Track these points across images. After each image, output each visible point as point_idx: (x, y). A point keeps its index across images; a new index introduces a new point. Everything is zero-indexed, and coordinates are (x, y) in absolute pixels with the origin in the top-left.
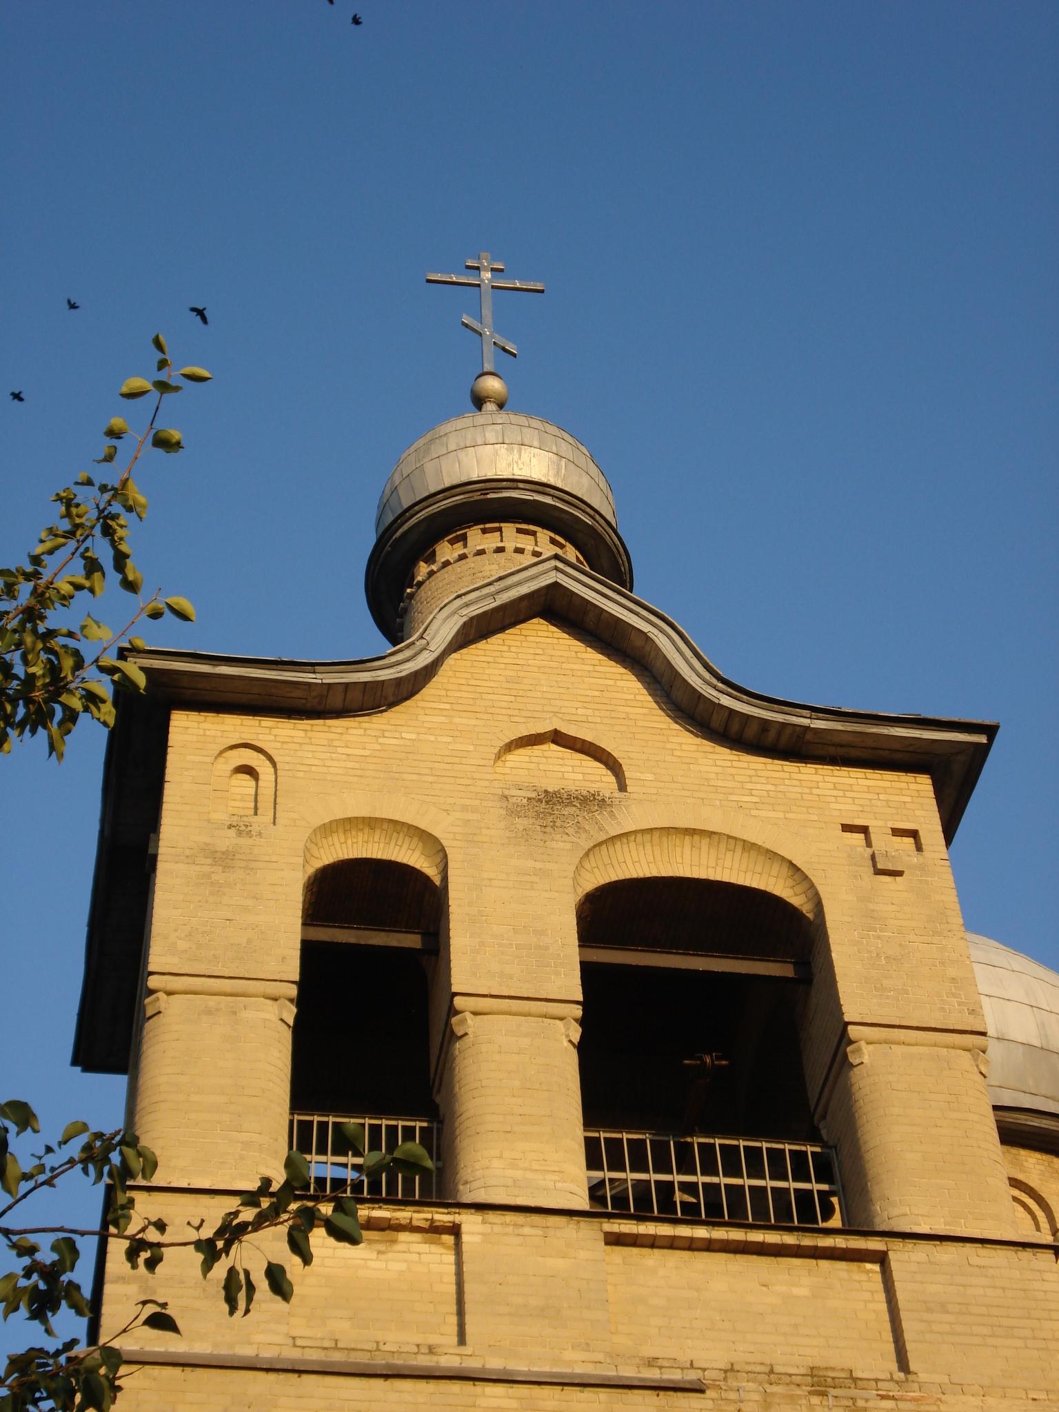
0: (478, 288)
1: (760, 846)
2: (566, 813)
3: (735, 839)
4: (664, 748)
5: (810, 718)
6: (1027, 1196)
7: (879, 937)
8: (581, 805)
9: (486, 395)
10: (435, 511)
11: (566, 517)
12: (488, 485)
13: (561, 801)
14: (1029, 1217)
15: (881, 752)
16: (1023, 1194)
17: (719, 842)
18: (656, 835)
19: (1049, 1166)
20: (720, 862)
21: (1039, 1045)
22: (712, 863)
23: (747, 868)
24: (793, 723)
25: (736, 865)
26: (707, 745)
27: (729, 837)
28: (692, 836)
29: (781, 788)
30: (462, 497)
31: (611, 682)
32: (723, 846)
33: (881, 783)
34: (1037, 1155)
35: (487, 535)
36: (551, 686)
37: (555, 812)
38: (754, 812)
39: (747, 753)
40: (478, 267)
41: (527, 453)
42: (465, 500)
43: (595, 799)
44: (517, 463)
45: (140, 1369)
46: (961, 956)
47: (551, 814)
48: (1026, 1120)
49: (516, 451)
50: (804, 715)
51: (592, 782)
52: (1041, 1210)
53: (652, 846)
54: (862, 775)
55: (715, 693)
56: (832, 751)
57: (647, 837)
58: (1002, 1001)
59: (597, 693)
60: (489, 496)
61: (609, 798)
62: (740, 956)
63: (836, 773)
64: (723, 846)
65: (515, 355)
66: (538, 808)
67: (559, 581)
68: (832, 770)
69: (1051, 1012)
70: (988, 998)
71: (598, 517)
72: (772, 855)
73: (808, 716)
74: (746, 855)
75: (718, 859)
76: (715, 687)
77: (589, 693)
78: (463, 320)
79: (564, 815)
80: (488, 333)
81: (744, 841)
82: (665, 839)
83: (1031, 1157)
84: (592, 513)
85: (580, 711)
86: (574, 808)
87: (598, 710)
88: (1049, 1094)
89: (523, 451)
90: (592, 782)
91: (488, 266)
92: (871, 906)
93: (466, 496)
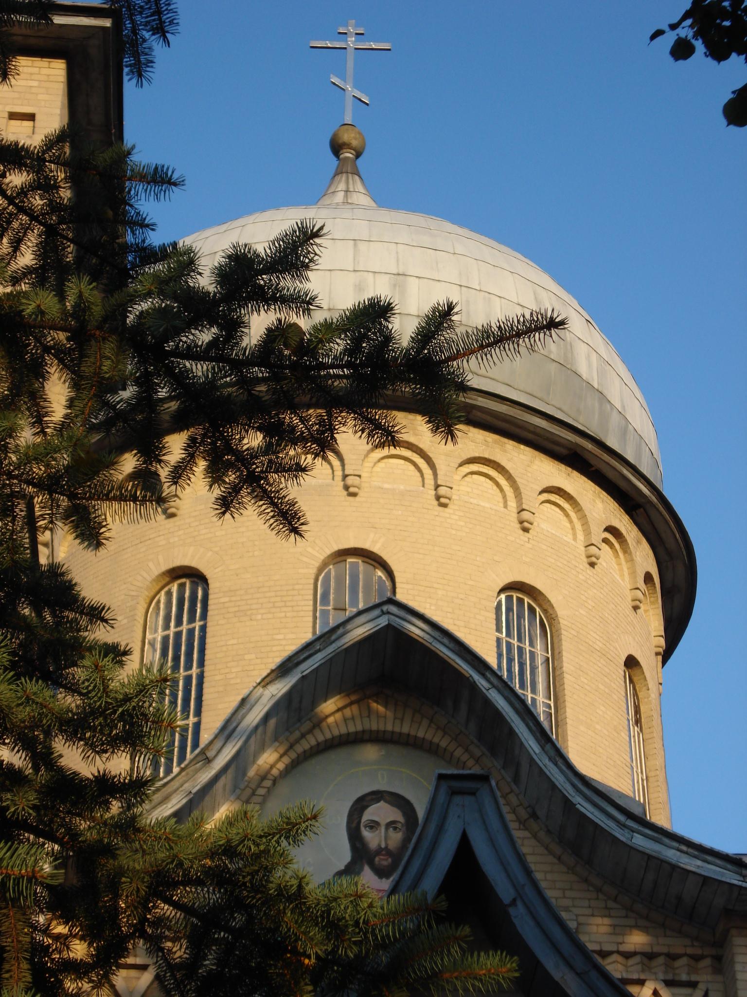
14: (418, 474)
16: (415, 455)
58: (431, 282)
65: (367, 104)
70: (417, 279)
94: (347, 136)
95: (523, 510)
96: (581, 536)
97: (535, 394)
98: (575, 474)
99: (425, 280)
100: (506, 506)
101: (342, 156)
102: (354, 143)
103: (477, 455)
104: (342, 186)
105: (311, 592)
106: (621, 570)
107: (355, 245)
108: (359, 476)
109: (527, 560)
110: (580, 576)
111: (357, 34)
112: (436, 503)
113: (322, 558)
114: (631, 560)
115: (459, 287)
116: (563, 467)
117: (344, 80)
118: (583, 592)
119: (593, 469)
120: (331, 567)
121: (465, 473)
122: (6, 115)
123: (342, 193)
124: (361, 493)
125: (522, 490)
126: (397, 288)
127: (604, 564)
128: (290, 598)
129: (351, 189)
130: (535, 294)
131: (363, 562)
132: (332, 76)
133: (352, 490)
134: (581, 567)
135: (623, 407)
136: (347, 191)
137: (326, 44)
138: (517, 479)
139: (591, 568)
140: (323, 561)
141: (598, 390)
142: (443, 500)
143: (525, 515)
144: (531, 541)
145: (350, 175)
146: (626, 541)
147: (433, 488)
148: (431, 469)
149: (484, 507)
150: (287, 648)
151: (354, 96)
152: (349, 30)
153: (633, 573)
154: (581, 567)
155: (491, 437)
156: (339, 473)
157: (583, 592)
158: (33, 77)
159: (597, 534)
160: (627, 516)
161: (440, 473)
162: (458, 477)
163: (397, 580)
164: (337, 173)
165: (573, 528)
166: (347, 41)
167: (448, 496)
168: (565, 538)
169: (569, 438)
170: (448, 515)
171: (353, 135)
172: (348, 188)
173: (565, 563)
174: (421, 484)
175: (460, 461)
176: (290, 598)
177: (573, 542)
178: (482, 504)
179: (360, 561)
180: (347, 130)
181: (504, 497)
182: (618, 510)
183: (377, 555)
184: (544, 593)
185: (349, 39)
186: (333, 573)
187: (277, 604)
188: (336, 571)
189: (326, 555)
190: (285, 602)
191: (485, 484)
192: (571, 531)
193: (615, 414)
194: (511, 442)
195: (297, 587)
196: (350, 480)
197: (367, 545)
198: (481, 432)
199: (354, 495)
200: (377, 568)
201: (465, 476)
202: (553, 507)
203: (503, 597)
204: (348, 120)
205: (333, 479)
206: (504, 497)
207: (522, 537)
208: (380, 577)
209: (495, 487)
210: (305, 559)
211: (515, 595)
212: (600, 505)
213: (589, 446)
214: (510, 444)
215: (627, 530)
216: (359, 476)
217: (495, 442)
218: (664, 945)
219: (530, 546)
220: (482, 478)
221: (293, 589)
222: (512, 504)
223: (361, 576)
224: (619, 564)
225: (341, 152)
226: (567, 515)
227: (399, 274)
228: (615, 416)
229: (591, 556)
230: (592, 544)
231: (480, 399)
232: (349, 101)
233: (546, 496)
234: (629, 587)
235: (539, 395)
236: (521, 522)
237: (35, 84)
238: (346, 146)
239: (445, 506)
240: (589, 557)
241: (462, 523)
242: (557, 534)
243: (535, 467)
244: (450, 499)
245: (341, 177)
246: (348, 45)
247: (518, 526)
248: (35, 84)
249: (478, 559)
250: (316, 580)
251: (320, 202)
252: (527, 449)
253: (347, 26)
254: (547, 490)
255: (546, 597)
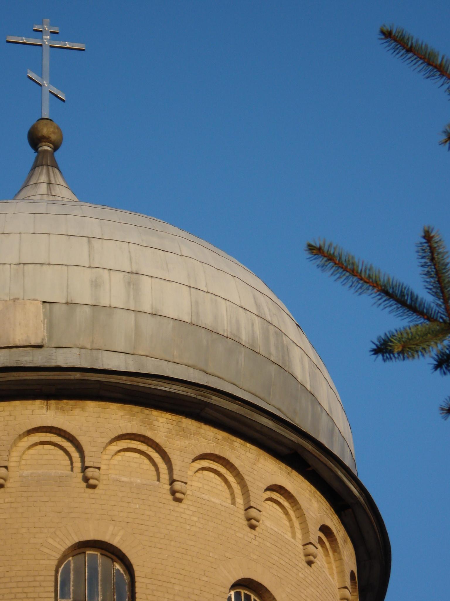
0: (41, 47)
6: (154, 451)
14: (153, 468)
16: (150, 449)
19: (177, 425)
21: (189, 321)
34: (168, 416)
40: (41, 30)
45: (317, 542)
48: (157, 385)
52: (164, 463)
58: (162, 281)
65: (63, 101)
69: (207, 292)
70: (150, 278)
78: (28, 75)
83: (161, 417)
88: (190, 363)
94: (45, 130)
95: (251, 507)
96: (299, 535)
97: (257, 394)
98: (294, 473)
99: (157, 279)
100: (234, 503)
101: (40, 149)
102: (53, 137)
103: (209, 451)
104: (43, 178)
105: (53, 584)
106: (330, 569)
107: (89, 242)
108: (99, 468)
109: (255, 557)
110: (300, 574)
111: (51, 32)
112: (171, 497)
113: (63, 549)
114: (339, 559)
115: (188, 288)
116: (283, 466)
117: (41, 77)
118: (303, 591)
119: (310, 469)
120: (70, 559)
121: (197, 469)
123: (45, 186)
124: (100, 486)
125: (250, 488)
126: (132, 286)
127: (319, 563)
128: (31, 590)
129: (53, 182)
130: (254, 298)
131: (101, 554)
132: (28, 71)
133: (92, 482)
134: (301, 565)
135: (330, 409)
136: (49, 183)
137: (65, 44)
138: (245, 477)
139: (309, 567)
140: (64, 552)
141: (310, 392)
142: (178, 495)
143: (253, 513)
144: (257, 538)
145: (50, 168)
146: (336, 540)
147: (168, 482)
148: (166, 464)
149: (215, 503)
151: (50, 92)
152: (44, 28)
153: (341, 572)
154: (301, 565)
155: (221, 435)
156: (78, 464)
157: (303, 591)
159: (315, 534)
160: (336, 516)
161: (176, 468)
162: (190, 473)
163: (137, 574)
164: (35, 166)
165: (292, 527)
166: (42, 39)
167: (183, 491)
168: (286, 536)
169: (293, 439)
170: (182, 510)
171: (51, 130)
172: (50, 180)
173: (287, 561)
174: (155, 478)
175: (193, 457)
176: (31, 590)
177: (293, 540)
178: (213, 500)
179: (99, 554)
180: (46, 124)
181: (232, 493)
182: (329, 509)
183: (116, 548)
184: (270, 589)
185: (44, 37)
186: (72, 566)
187: (19, 596)
188: (75, 563)
189: (67, 547)
190: (27, 593)
191: (214, 480)
192: (289, 529)
193: (324, 415)
194: (239, 440)
195: (38, 578)
196: (90, 472)
197: (106, 538)
198: (212, 429)
199: (94, 487)
200: (116, 562)
201: (196, 472)
202: (274, 505)
203: (232, 593)
204: (46, 114)
205: (72, 470)
206: (232, 493)
207: (249, 534)
208: (118, 570)
209: (223, 484)
210: (46, 550)
211: (243, 592)
212: (315, 505)
213: (310, 447)
214: (238, 442)
215: (336, 528)
216: (99, 468)
217: (224, 439)
219: (256, 543)
220: (212, 475)
221: (35, 581)
222: (240, 500)
223: (99, 569)
224: (329, 563)
225: (40, 145)
226: (287, 514)
227: (132, 273)
228: (324, 417)
229: (309, 555)
230: (310, 543)
231: (214, 397)
232: (46, 97)
233: (269, 494)
234: (338, 585)
235: (262, 396)
236: (249, 519)
238: (46, 139)
239: (179, 500)
240: (307, 555)
241: (195, 519)
242: (280, 532)
243: (260, 465)
244: (184, 494)
245: (42, 170)
246: (44, 42)
247: (246, 523)
249: (211, 555)
250: (57, 571)
251: (23, 194)
252: (253, 447)
253: (42, 24)
254: (271, 488)
255: (271, 594)
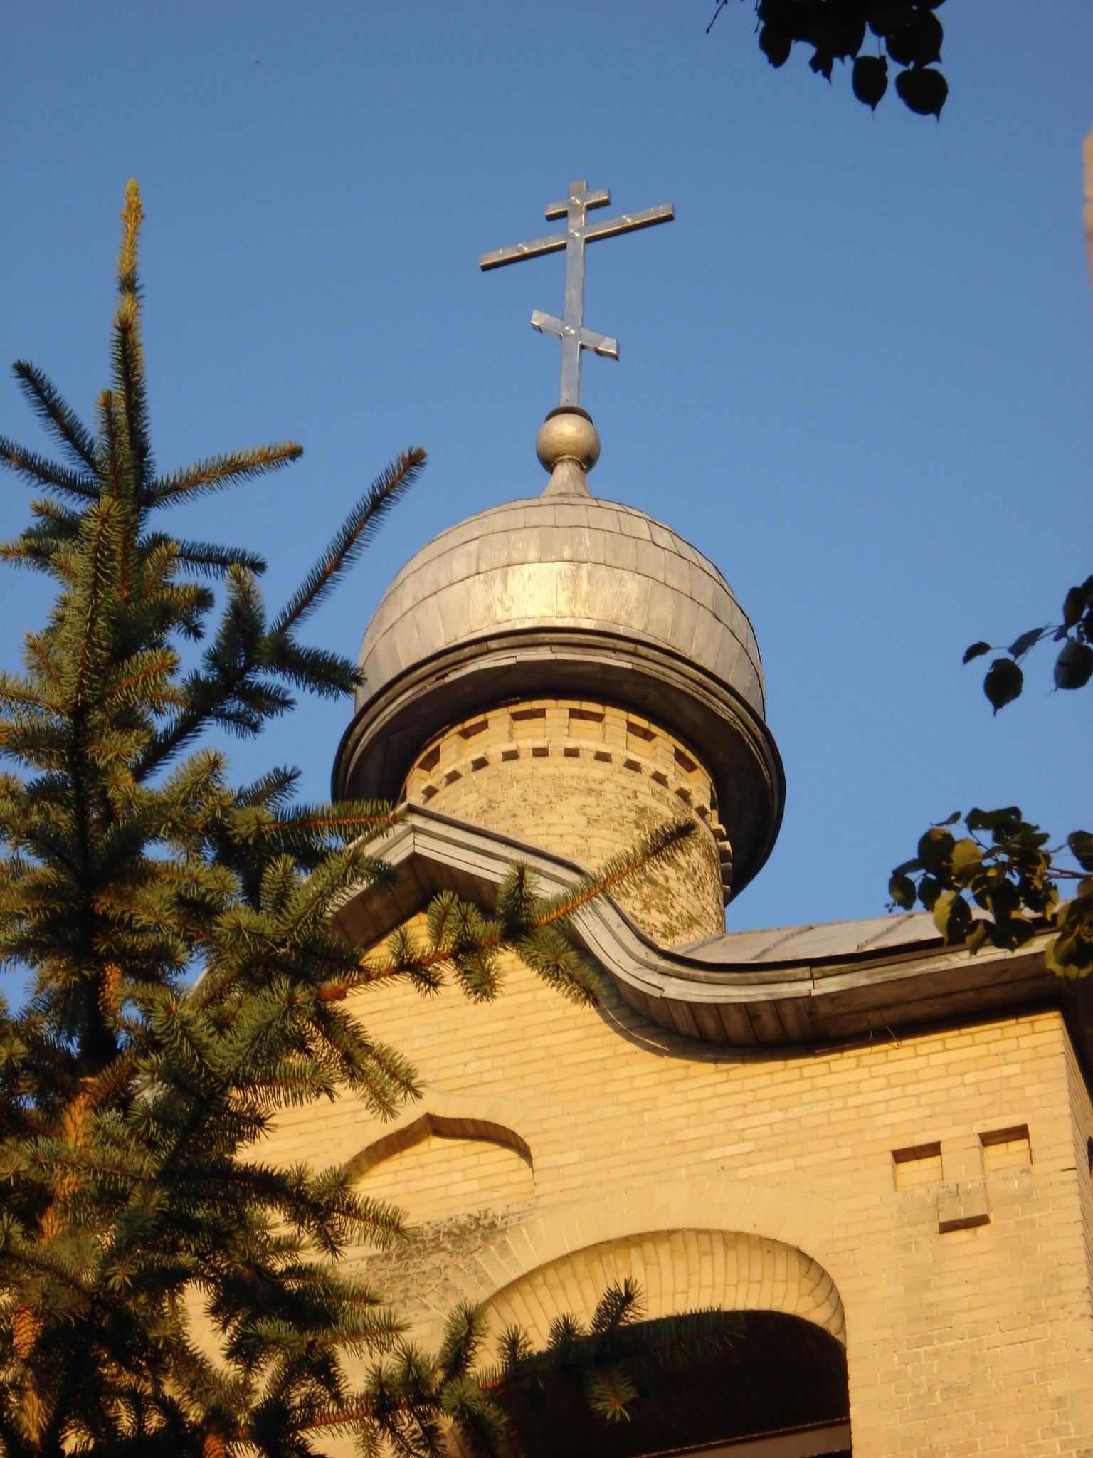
1: (748, 1234)
2: (427, 1267)
3: (708, 1232)
4: (396, 1172)
5: (812, 978)
7: (936, 1354)
8: (454, 1245)
9: (554, 452)
10: (381, 725)
11: (589, 668)
12: (443, 661)
13: (421, 1247)
15: (961, 997)
17: (685, 1245)
18: (580, 1262)
20: (694, 1279)
22: (681, 1285)
23: (738, 1277)
24: (786, 996)
25: (720, 1278)
26: (676, 1065)
27: (698, 1232)
28: (669, 1240)
29: (795, 1112)
30: (410, 692)
31: (526, 997)
32: (693, 1249)
33: (970, 1052)
35: (473, 739)
36: (429, 1036)
37: (411, 1271)
38: (744, 1173)
39: (743, 1061)
41: (519, 577)
42: (414, 698)
43: (478, 1225)
44: (501, 601)
46: (1078, 1350)
47: (402, 1277)
49: (498, 580)
50: (800, 976)
51: (492, 1189)
53: (579, 1283)
54: (939, 1046)
55: (655, 979)
56: (875, 1019)
57: (566, 1270)
59: (500, 1025)
60: (447, 680)
61: (502, 1218)
62: (739, 1438)
63: (894, 1054)
64: (693, 1249)
66: (383, 1272)
67: (419, 850)
68: (886, 1051)
71: (643, 650)
72: (769, 1245)
73: (807, 976)
74: (732, 1255)
75: (689, 1274)
76: (655, 968)
77: (489, 1028)
79: (424, 1273)
80: (573, 332)
81: (722, 1232)
82: (596, 1264)
84: (630, 647)
85: (471, 1068)
86: (443, 1255)
87: (499, 1056)
89: (510, 576)
90: (492, 1189)
91: (582, 203)
92: (929, 1297)
93: (416, 688)
111: (591, 207)
122: (977, 1141)
150: (389, 1178)
158: (1009, 1058)
218: (700, 1263)
237: (1015, 1069)
248: (1015, 1069)
